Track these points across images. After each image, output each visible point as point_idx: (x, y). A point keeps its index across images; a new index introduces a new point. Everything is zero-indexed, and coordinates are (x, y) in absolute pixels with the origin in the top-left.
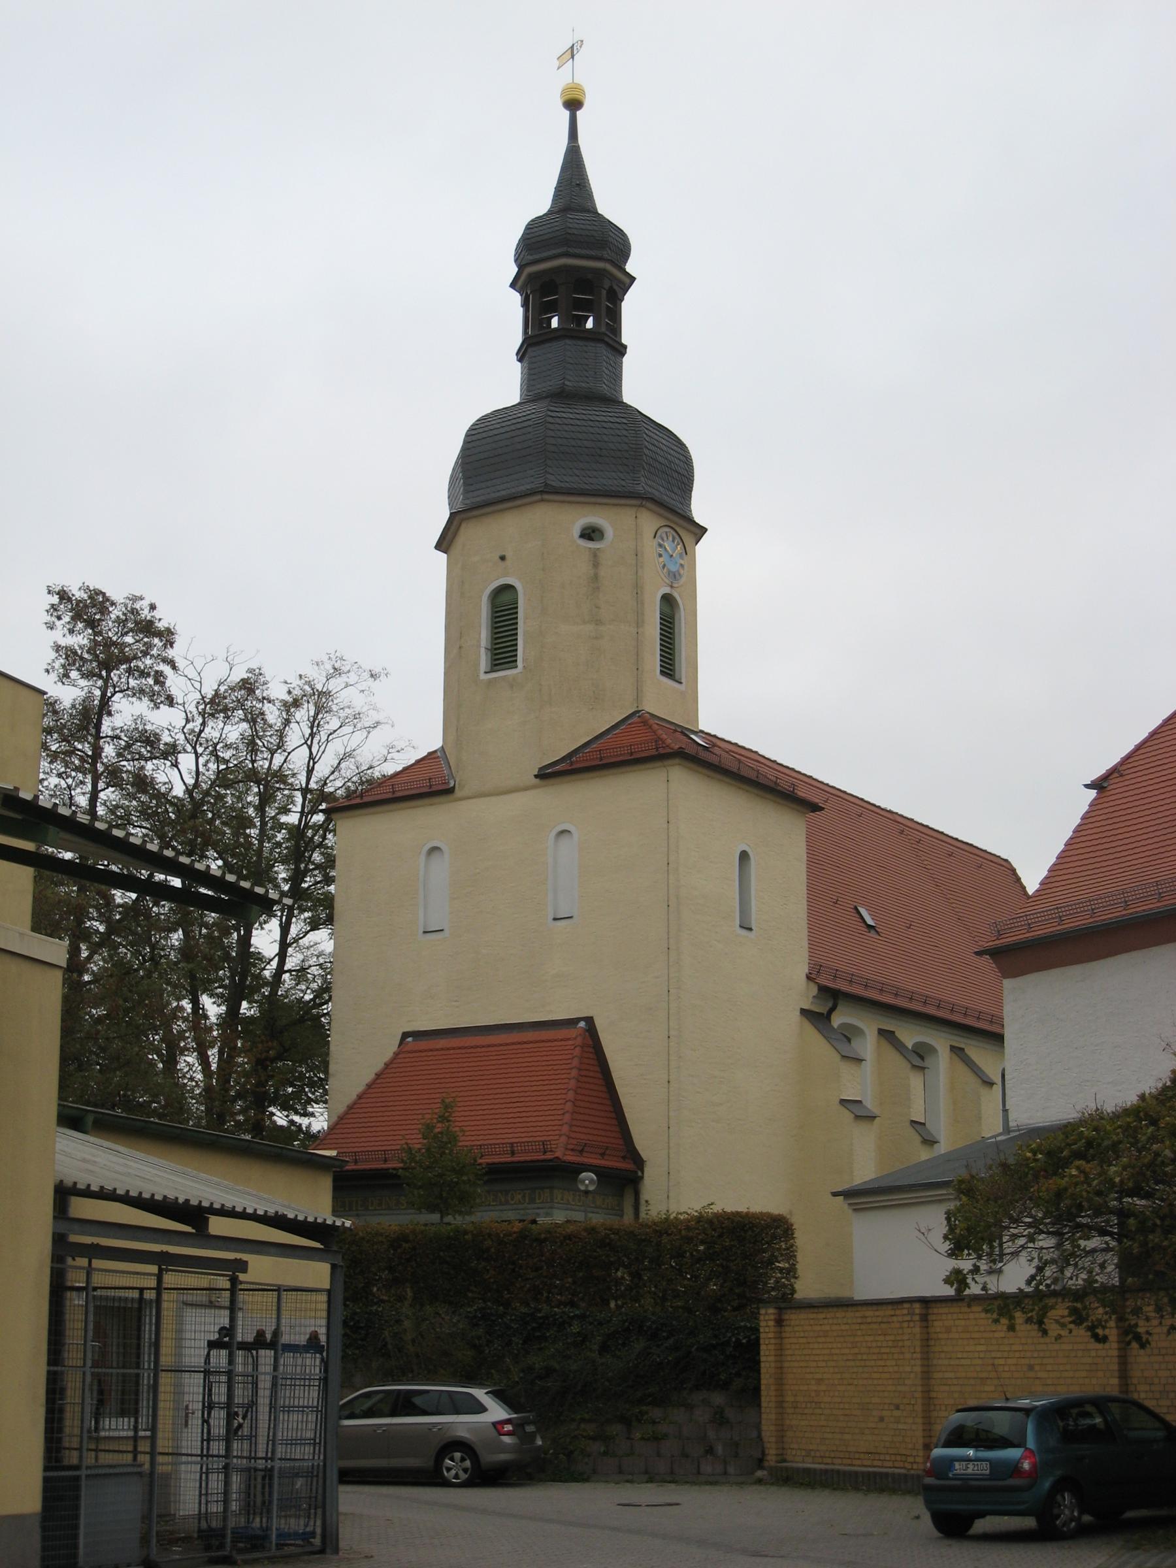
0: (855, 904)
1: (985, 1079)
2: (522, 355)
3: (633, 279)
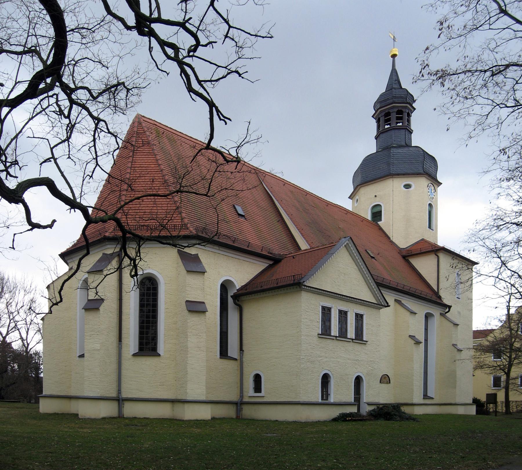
0: (234, 204)
1: (411, 311)
2: (376, 138)
3: (415, 109)
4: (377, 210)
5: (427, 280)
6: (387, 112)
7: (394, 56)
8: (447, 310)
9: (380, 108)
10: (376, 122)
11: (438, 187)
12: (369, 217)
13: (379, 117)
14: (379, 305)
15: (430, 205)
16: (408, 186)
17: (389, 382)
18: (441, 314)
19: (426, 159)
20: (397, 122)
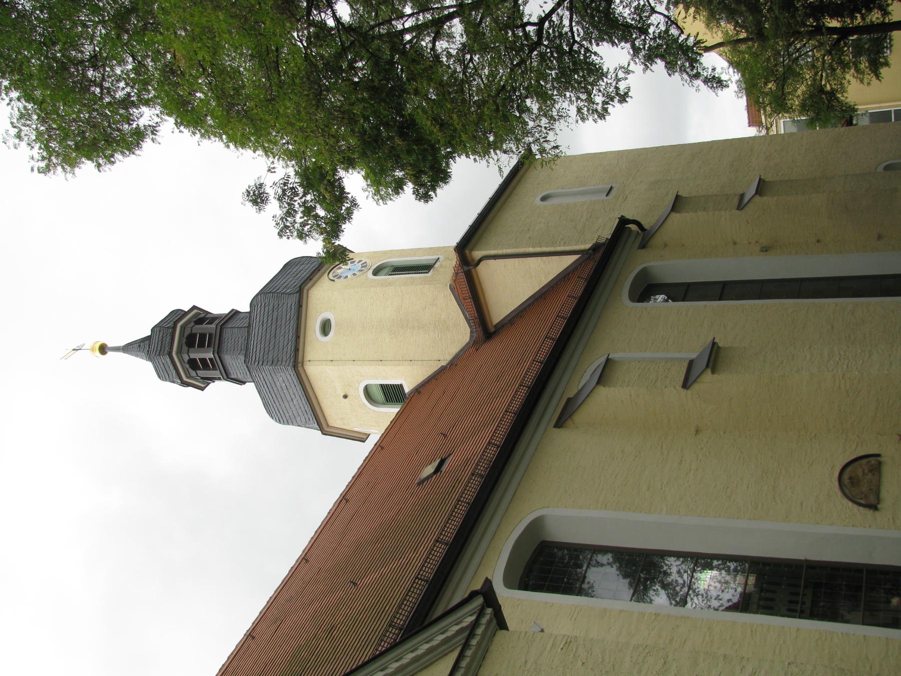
4: (379, 395)
5: (549, 279)
6: (187, 366)
7: (103, 349)
8: (633, 227)
10: (214, 382)
12: (392, 411)
14: (466, 645)
15: (376, 272)
16: (326, 328)
17: (873, 461)
18: (643, 246)
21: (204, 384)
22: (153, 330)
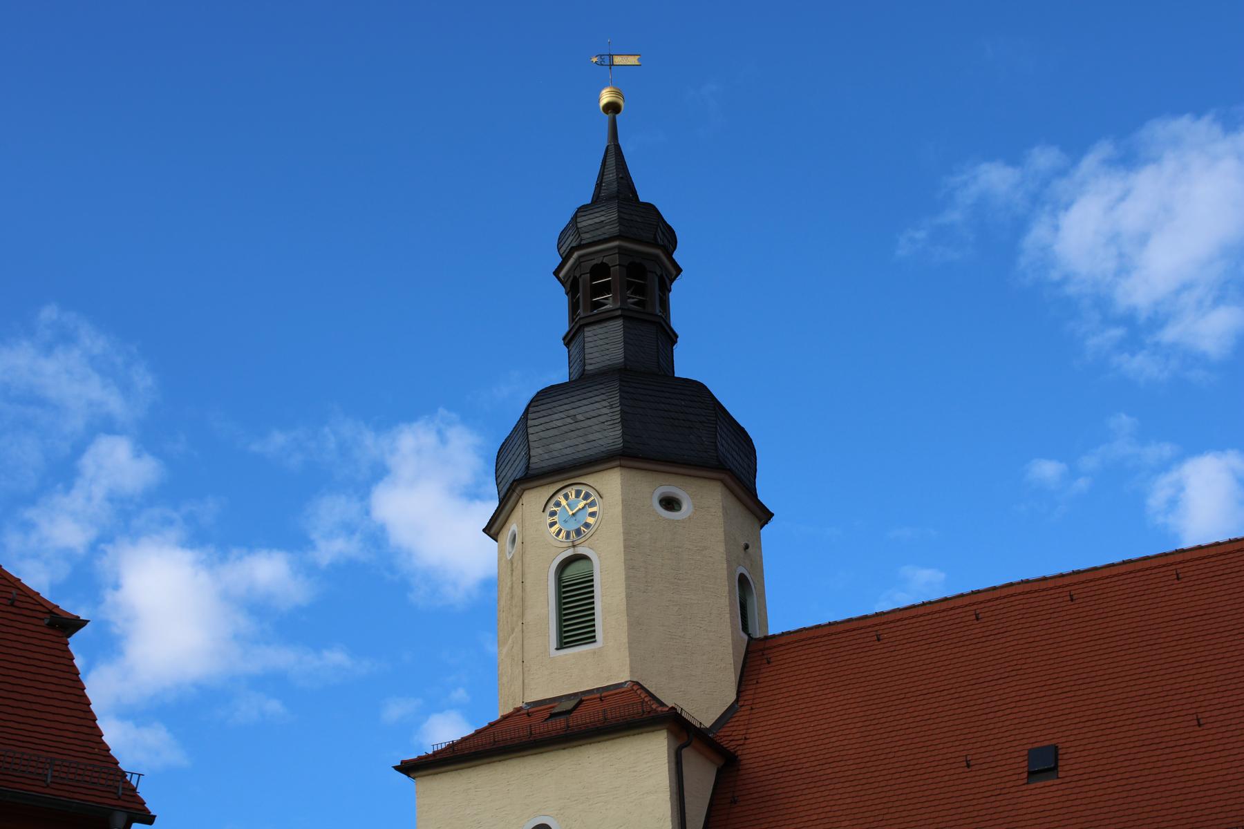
4: (574, 571)
9: (580, 247)
10: (567, 294)
11: (762, 527)
13: (575, 277)
16: (670, 503)
19: (721, 428)
20: (628, 281)
21: (564, 278)
22: (650, 208)
